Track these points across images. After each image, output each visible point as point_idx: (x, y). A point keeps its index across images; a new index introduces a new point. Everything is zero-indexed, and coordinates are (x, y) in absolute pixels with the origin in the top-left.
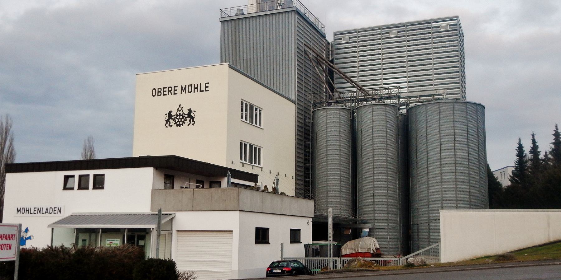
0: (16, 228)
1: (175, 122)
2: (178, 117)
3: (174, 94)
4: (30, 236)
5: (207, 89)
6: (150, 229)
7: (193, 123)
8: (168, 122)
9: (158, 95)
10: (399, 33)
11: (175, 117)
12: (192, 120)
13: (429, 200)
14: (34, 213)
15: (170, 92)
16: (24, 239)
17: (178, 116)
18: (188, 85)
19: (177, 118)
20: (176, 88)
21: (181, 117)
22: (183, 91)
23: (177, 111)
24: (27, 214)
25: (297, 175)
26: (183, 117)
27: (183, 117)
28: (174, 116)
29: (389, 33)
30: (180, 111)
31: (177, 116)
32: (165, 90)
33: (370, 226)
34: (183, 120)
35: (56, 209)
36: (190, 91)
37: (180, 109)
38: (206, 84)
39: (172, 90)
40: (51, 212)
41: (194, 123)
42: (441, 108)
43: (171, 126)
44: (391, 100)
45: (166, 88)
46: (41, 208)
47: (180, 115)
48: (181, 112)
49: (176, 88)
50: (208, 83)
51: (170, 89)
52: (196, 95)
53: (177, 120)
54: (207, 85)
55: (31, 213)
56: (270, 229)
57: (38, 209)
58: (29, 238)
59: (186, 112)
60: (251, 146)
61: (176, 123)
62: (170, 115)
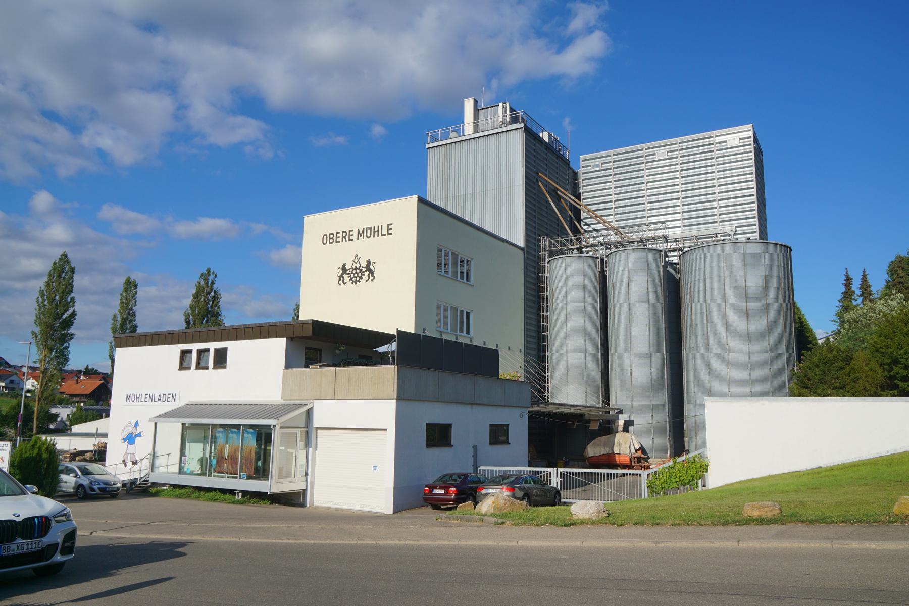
0: (593, 399)
2: (354, 272)
3: (350, 240)
4: (140, 433)
5: (390, 232)
6: (270, 425)
8: (342, 278)
9: (330, 243)
10: (668, 154)
13: (710, 381)
14: (145, 402)
15: (344, 238)
16: (134, 435)
18: (367, 228)
19: (352, 273)
20: (351, 233)
21: (358, 271)
22: (361, 237)
24: (138, 403)
25: (526, 348)
27: (361, 270)
29: (654, 154)
30: (356, 263)
31: (353, 269)
32: (338, 235)
33: (626, 417)
34: (360, 275)
35: (148, 396)
36: (369, 235)
37: (356, 261)
38: (388, 225)
39: (347, 236)
40: (164, 400)
41: (374, 278)
43: (345, 283)
44: (670, 248)
45: (340, 233)
47: (356, 268)
48: (358, 265)
49: (351, 233)
50: (391, 224)
51: (344, 234)
52: (376, 240)
53: (352, 276)
54: (390, 227)
55: (141, 402)
56: (453, 426)
57: (173, 396)
58: (139, 435)
59: (364, 264)
60: (455, 309)
61: (351, 279)
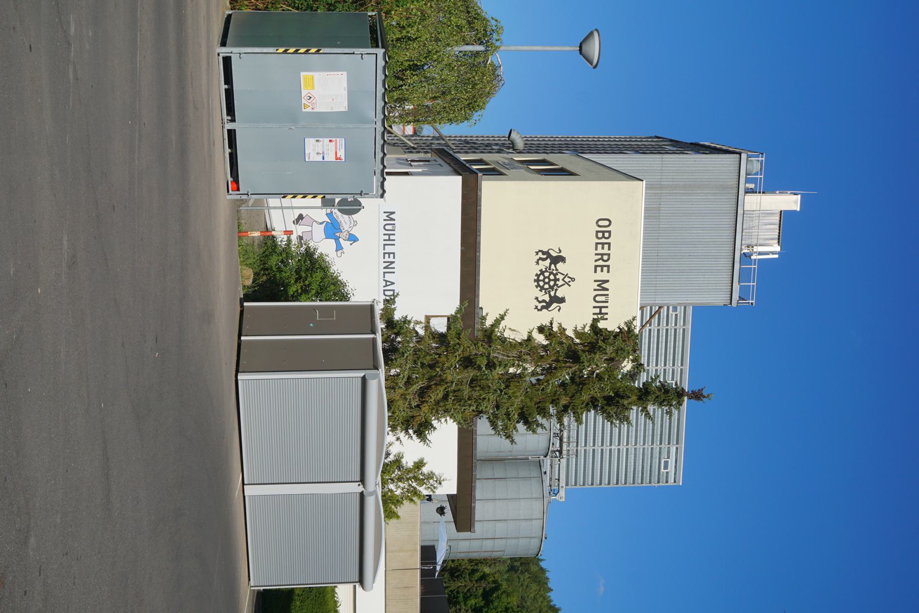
1: (544, 270)
2: (552, 277)
3: (596, 267)
4: (342, 248)
7: (539, 308)
8: (545, 256)
11: (553, 270)
12: (544, 304)
14: (384, 253)
15: (600, 257)
17: (555, 277)
18: (608, 295)
20: (605, 269)
23: (563, 275)
26: (551, 288)
27: (551, 288)
28: (555, 267)
30: (563, 280)
31: (555, 275)
35: (391, 259)
37: (567, 280)
39: (603, 262)
41: (539, 310)
42: (534, 522)
43: (537, 263)
45: (609, 249)
46: (394, 268)
48: (560, 283)
49: (605, 269)
50: (608, 271)
61: (542, 272)
62: (560, 259)
